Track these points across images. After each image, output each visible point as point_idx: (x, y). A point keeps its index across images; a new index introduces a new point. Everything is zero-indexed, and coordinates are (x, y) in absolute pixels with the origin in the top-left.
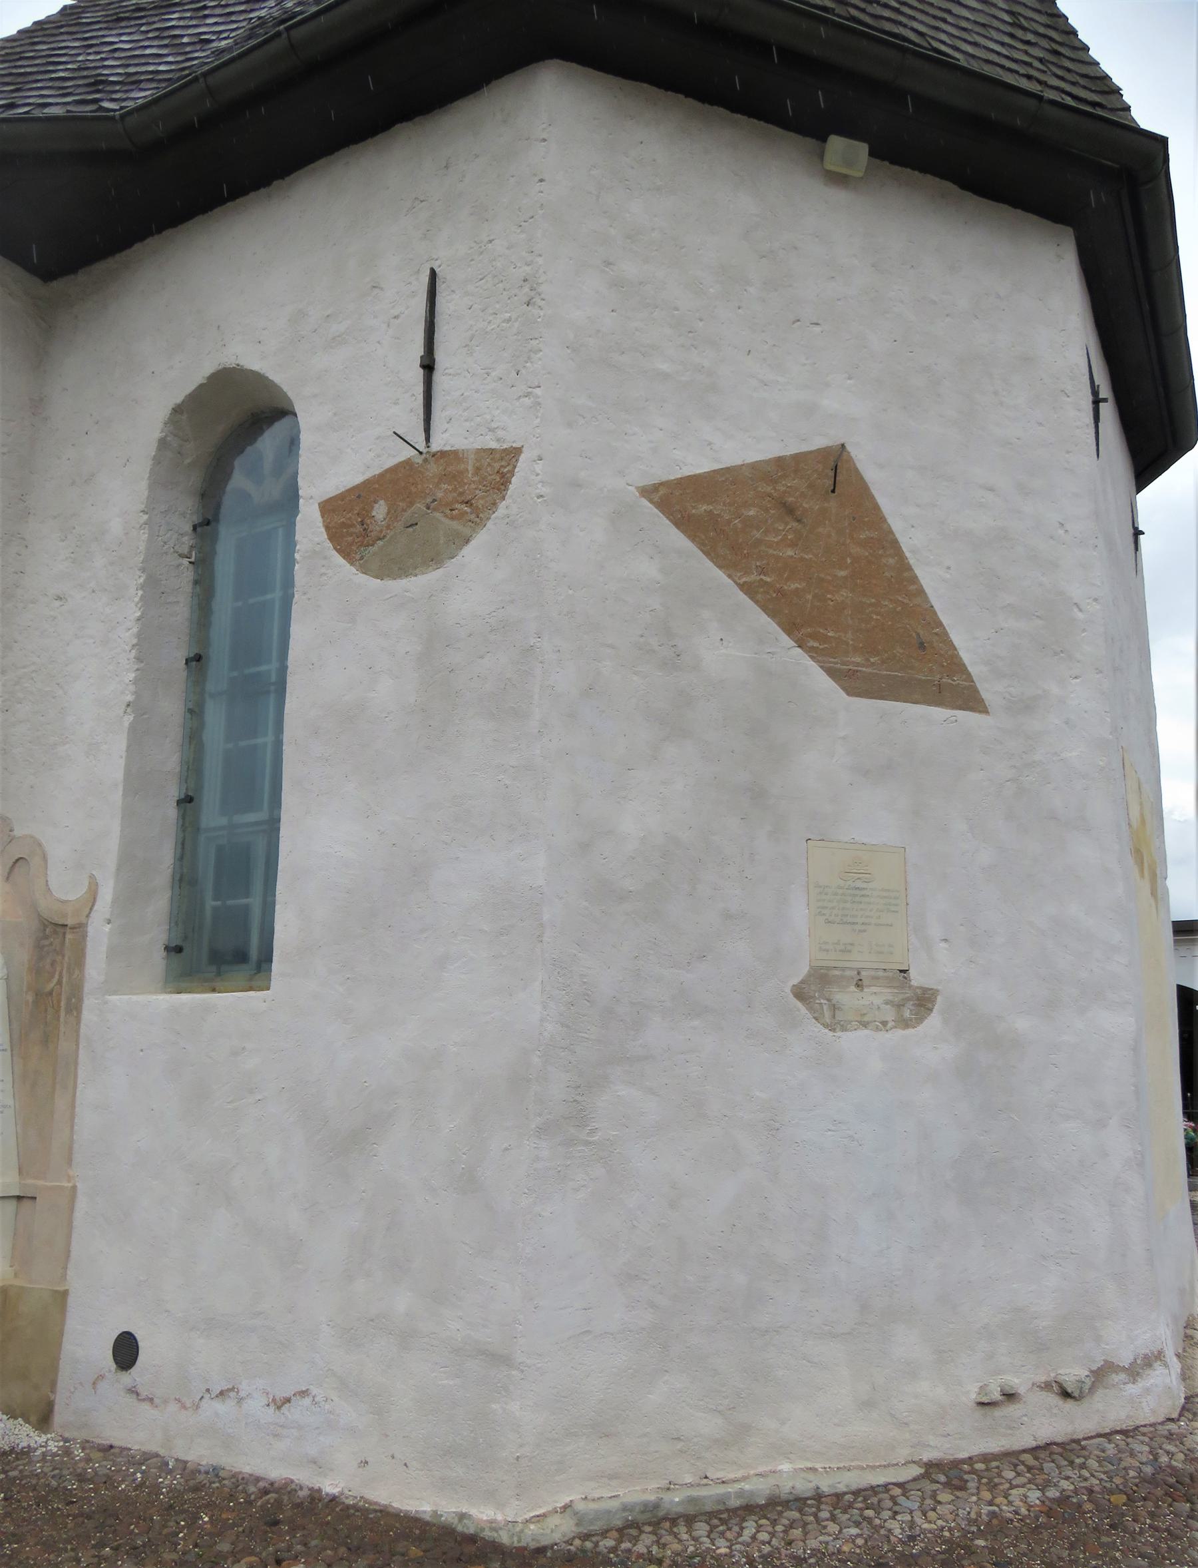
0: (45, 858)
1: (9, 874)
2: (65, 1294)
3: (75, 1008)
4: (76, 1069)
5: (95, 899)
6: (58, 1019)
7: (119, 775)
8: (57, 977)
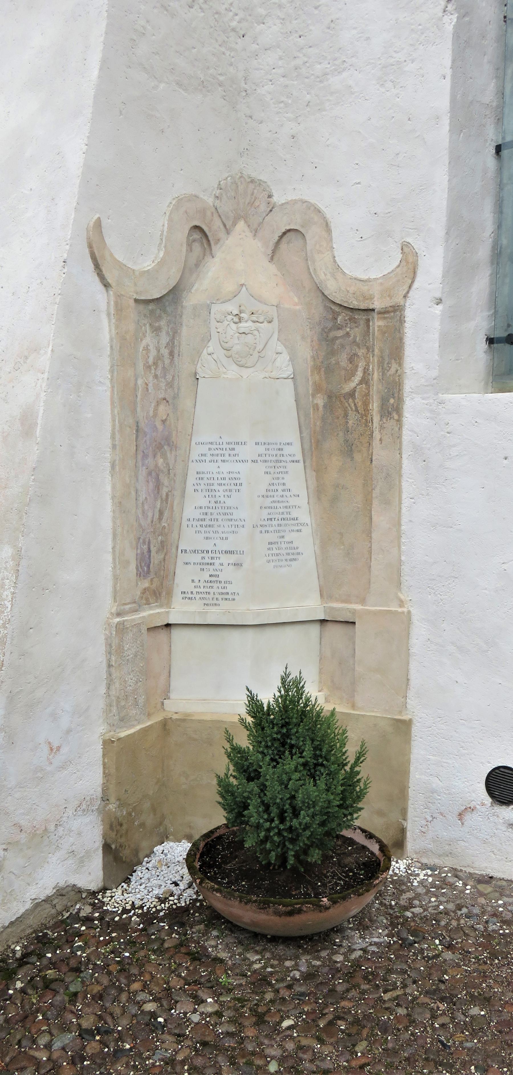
0: (327, 227)
1: (274, 252)
3: (392, 408)
4: (400, 482)
5: (415, 273)
7: (443, 103)
8: (360, 374)
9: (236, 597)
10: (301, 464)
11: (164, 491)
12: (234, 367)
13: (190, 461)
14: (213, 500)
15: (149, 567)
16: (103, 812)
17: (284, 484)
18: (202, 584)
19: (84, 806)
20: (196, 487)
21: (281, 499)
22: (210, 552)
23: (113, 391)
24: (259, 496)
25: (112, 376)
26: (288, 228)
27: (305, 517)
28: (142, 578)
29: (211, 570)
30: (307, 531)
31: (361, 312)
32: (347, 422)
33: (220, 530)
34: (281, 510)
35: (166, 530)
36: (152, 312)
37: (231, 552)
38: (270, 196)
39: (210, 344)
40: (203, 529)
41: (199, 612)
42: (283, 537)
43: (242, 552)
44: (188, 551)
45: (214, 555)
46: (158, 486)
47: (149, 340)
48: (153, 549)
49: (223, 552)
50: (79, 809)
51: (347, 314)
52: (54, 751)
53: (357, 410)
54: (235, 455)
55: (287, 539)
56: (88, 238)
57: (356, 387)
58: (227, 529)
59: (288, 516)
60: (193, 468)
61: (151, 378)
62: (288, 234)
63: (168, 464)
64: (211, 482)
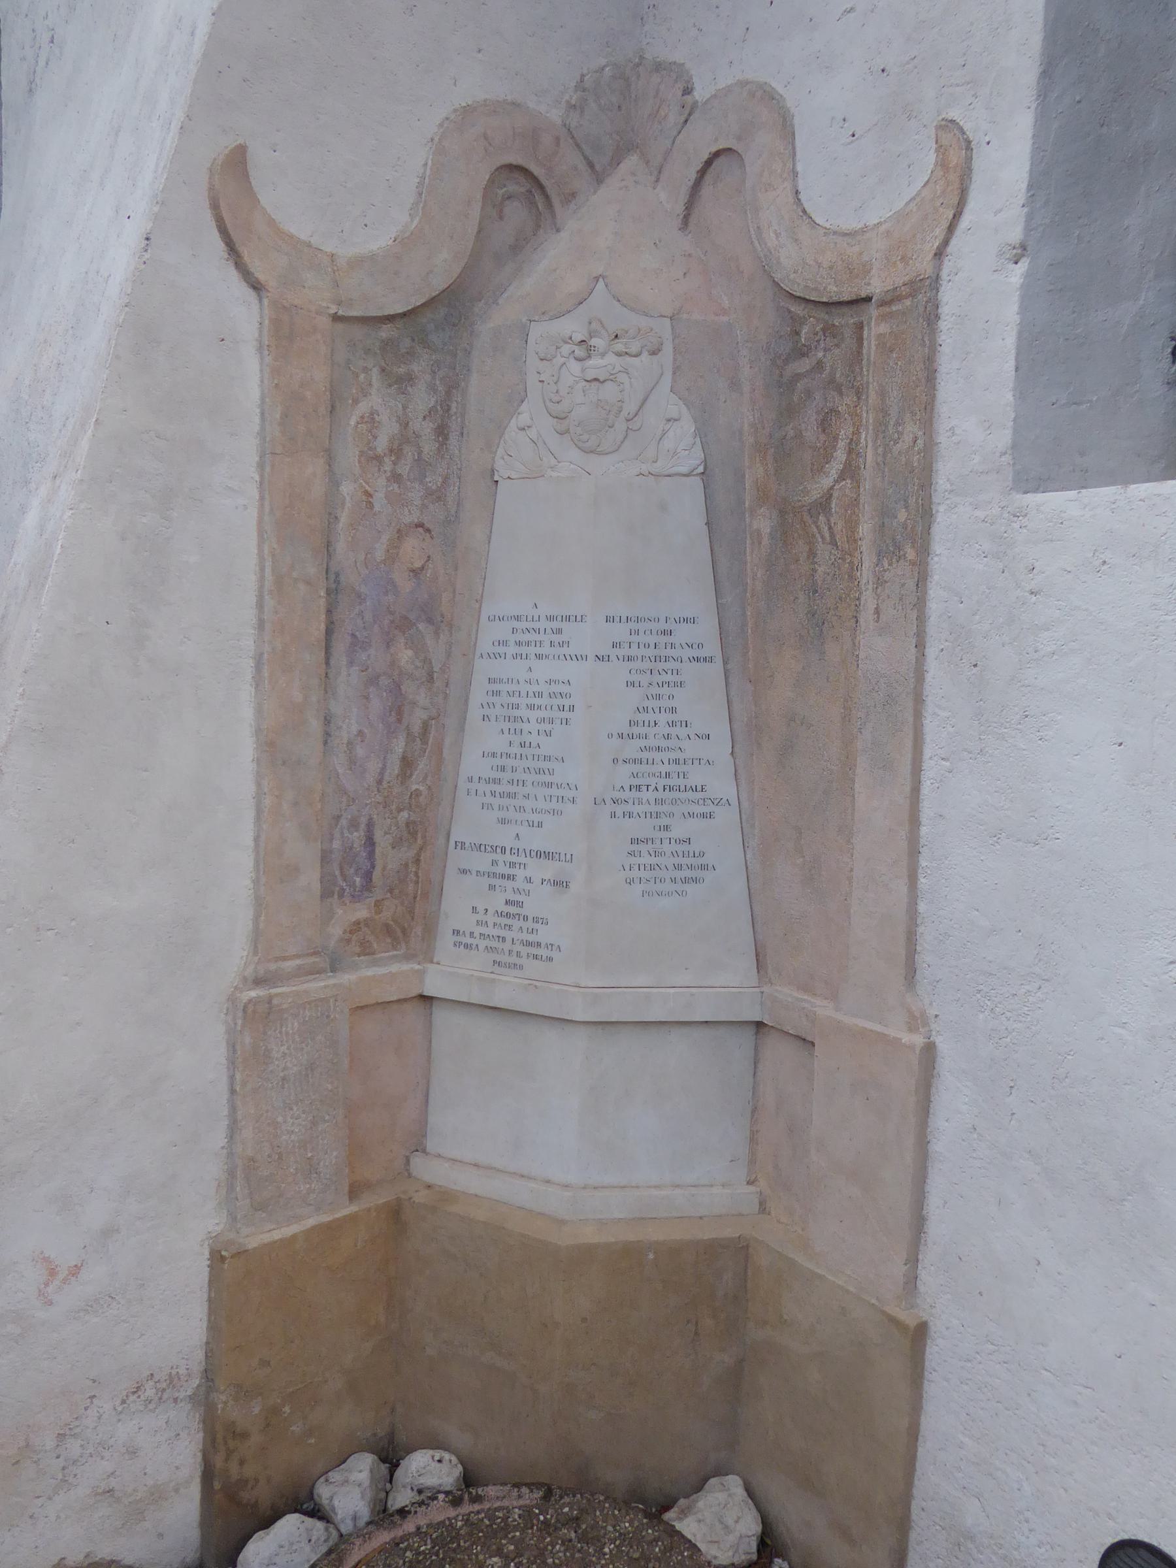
1: (689, 206)
2: (920, 1333)
3: (909, 540)
4: (918, 715)
6: (854, 569)
8: (840, 455)
9: (554, 954)
10: (718, 666)
11: (416, 718)
12: (574, 454)
13: (478, 654)
14: (517, 739)
15: (368, 876)
16: (205, 1402)
17: (673, 710)
18: (491, 919)
19: (149, 1392)
20: (487, 711)
21: (664, 743)
22: (508, 851)
23: (262, 506)
24: (610, 736)
25: (262, 476)
26: (714, 149)
27: (722, 786)
28: (347, 900)
29: (510, 890)
30: (727, 817)
31: (845, 310)
32: (815, 570)
33: (528, 804)
34: (664, 769)
35: (421, 799)
36: (387, 345)
37: (548, 855)
38: (687, 91)
39: (524, 407)
40: (496, 802)
41: (480, 979)
42: (667, 828)
43: (568, 857)
44: (467, 845)
45: (514, 859)
46: (398, 709)
47: (377, 400)
48: (382, 841)
49: (533, 854)
50: (132, 1398)
51: (818, 320)
52: (61, 1276)
53: (834, 543)
54: (561, 645)
55: (677, 832)
56: (211, 188)
57: (832, 488)
58: (541, 804)
59: (681, 782)
60: (483, 669)
61: (382, 481)
62: (717, 163)
63: (427, 661)
64: (515, 700)
